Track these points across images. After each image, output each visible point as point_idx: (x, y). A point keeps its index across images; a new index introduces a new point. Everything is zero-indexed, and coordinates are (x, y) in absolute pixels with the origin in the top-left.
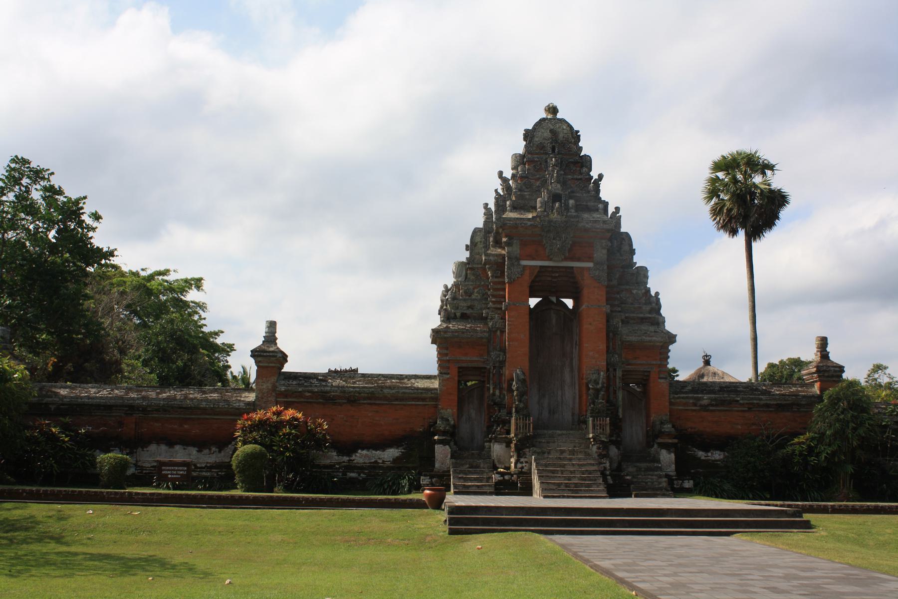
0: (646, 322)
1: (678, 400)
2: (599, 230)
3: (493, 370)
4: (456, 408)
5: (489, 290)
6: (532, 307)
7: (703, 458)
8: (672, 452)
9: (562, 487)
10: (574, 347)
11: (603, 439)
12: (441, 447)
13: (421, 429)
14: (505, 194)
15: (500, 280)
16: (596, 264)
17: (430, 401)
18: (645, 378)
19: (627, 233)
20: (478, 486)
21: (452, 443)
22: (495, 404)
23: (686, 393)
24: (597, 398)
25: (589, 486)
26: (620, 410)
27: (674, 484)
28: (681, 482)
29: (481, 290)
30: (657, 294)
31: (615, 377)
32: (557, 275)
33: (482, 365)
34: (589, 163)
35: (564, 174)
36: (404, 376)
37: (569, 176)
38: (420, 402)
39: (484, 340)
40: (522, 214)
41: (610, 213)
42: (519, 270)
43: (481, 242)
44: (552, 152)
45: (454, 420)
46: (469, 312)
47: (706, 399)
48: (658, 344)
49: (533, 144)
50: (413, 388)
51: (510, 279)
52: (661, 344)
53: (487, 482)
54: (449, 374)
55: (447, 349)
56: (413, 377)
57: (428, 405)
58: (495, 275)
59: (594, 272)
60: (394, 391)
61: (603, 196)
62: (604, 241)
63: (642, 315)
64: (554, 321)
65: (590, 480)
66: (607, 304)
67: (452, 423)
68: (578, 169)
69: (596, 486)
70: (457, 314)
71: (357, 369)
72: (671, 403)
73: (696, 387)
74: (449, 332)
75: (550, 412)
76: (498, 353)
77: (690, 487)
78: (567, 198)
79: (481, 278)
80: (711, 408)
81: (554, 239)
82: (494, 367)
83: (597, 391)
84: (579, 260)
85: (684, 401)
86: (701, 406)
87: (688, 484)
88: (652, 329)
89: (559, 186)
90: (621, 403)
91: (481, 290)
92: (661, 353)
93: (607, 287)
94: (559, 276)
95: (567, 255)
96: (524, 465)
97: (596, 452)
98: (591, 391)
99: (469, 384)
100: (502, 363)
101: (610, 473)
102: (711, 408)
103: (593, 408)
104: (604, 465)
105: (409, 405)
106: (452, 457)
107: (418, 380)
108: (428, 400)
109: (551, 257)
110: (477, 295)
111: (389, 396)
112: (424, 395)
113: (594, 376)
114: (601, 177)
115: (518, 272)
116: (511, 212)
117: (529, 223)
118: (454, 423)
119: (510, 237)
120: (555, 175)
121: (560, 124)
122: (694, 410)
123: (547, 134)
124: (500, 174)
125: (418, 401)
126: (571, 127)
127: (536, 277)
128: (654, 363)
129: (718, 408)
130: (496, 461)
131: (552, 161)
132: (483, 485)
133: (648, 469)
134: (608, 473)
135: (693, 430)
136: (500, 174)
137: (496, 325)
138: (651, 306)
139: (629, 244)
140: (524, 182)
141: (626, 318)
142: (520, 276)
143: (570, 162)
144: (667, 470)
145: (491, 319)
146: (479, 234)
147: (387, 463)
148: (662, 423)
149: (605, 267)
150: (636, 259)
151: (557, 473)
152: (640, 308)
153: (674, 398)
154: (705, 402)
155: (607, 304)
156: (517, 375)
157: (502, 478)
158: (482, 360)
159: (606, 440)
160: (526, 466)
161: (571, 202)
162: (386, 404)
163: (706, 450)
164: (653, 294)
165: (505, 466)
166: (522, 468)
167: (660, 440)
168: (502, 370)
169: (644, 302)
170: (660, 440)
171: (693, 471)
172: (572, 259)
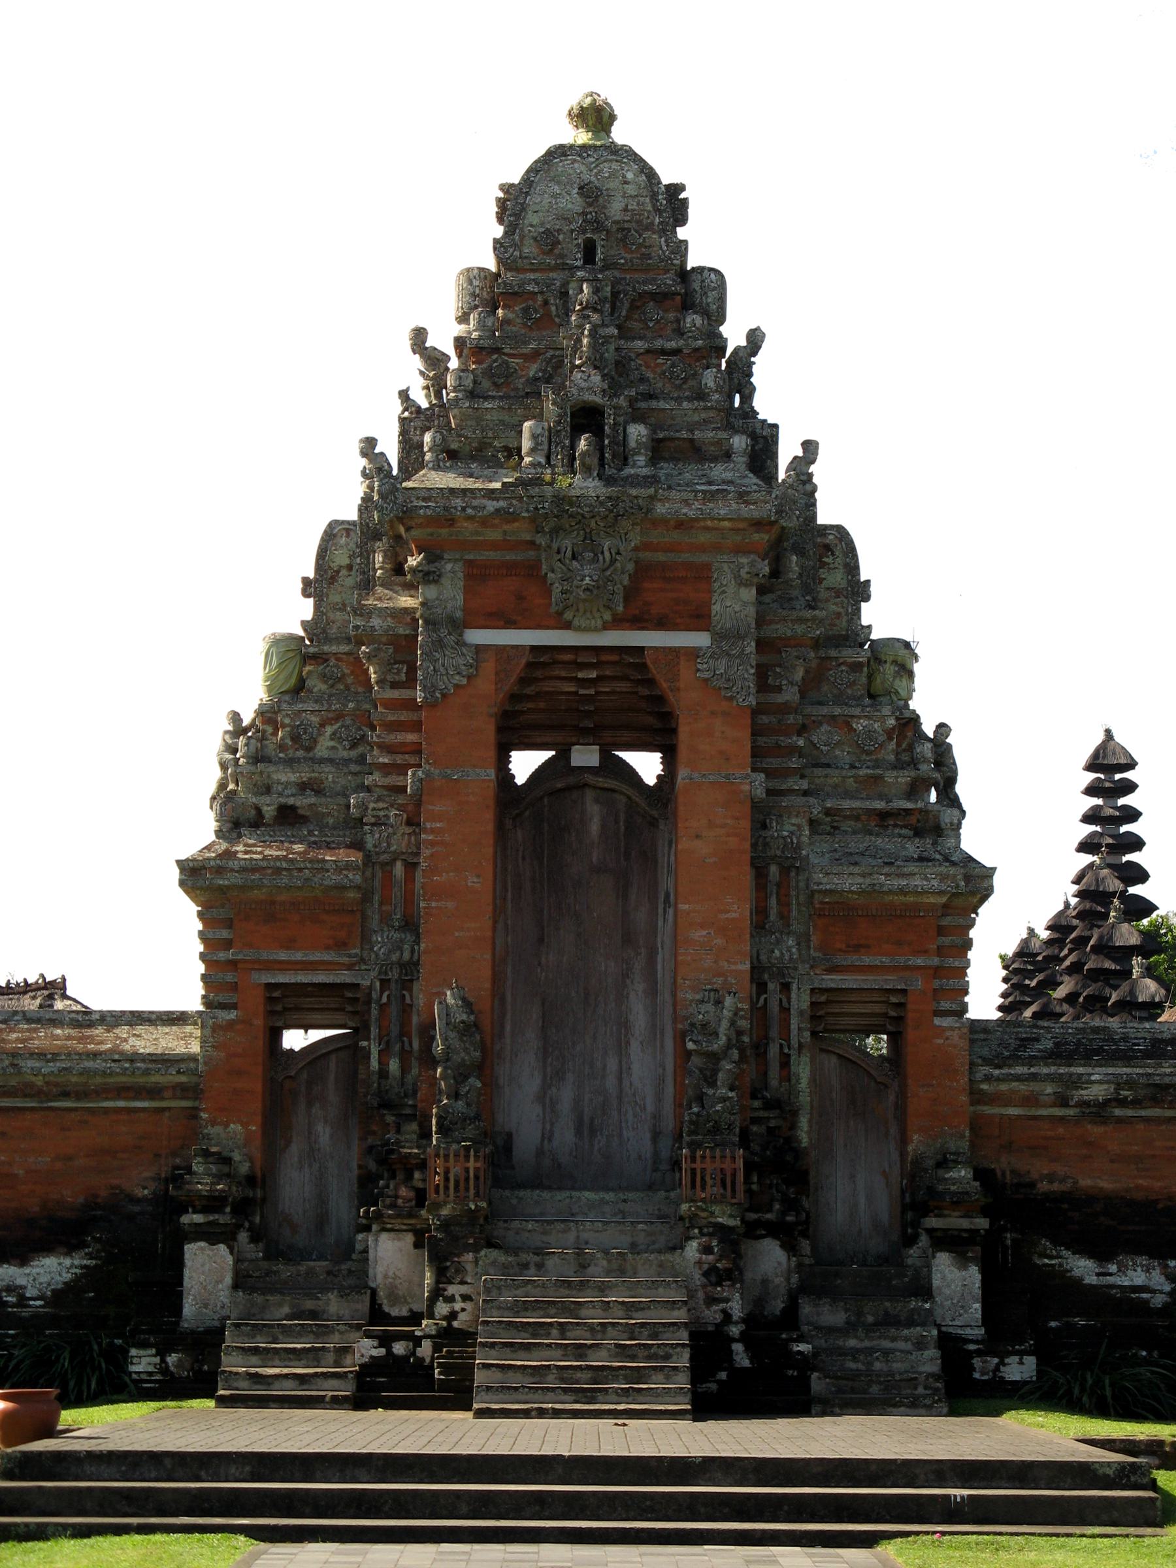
0: (895, 826)
1: (1004, 1087)
2: (726, 524)
3: (382, 992)
4: (259, 1119)
5: (373, 728)
6: (520, 780)
7: (1092, 1280)
8: (972, 1260)
9: (551, 1382)
10: (661, 911)
11: (720, 1220)
12: (202, 1249)
13: (146, 1192)
14: (432, 406)
15: (403, 694)
16: (719, 637)
17: (174, 1097)
18: (893, 1013)
19: (841, 533)
20: (302, 1379)
21: (243, 1236)
22: (386, 1105)
23: (1031, 1061)
24: (713, 1084)
25: (639, 1375)
26: (804, 1122)
27: (974, 1369)
28: (996, 1360)
29: (347, 727)
30: (943, 729)
31: (785, 1010)
32: (593, 675)
33: (345, 977)
34: (713, 295)
35: (620, 337)
36: (95, 1017)
37: (639, 343)
38: (143, 1099)
39: (352, 895)
40: (471, 476)
41: (784, 461)
42: (461, 661)
43: (350, 567)
44: (585, 262)
45: (251, 1160)
46: (302, 802)
47: (1100, 1082)
48: (932, 900)
49: (522, 238)
50: (116, 1057)
51: (432, 693)
52: (944, 899)
53: (337, 1364)
54: (234, 1006)
55: (229, 924)
56: (128, 1017)
57: (169, 1109)
58: (389, 678)
59: (711, 662)
60: (52, 1067)
61: (765, 407)
62: (744, 560)
63: (879, 805)
64: (595, 827)
65: (649, 1358)
66: (754, 770)
67: (244, 1169)
68: (671, 316)
69: (660, 1377)
70: (265, 809)
71: (64, 979)
72: (977, 1097)
73: (1067, 1043)
74: (232, 870)
75: (579, 1132)
76: (397, 935)
77: (1026, 1376)
78: (621, 419)
79: (347, 688)
80: (1118, 1112)
81: (574, 557)
82: (382, 981)
83: (714, 1058)
84: (662, 624)
85: (1022, 1087)
86: (1083, 1104)
87: (1020, 1369)
88: (912, 848)
89: (596, 378)
90: (804, 1098)
91: (347, 727)
92: (941, 931)
93: (756, 712)
94: (599, 678)
95: (621, 609)
96: (458, 1306)
97: (699, 1263)
98: (696, 1060)
99: (294, 1039)
100: (409, 971)
101: (742, 1333)
102: (1118, 1112)
103: (698, 1115)
104: (722, 1306)
105: (106, 1111)
106: (236, 1286)
107: (140, 1029)
108: (166, 1094)
109: (568, 615)
110: (332, 743)
111: (39, 1081)
112: (155, 1078)
113: (704, 1008)
114: (755, 339)
115: (456, 668)
116: (437, 467)
117: (491, 505)
118: (252, 1168)
119: (433, 555)
120: (585, 341)
121: (615, 166)
122: (1062, 1119)
123: (572, 202)
124: (419, 337)
125: (134, 1099)
126: (650, 175)
127: (523, 681)
128: (920, 961)
129: (1143, 1113)
130: (381, 1293)
131: (582, 291)
132: (316, 1375)
133: (889, 1321)
134: (735, 1331)
135: (1056, 1187)
136: (419, 337)
137: (389, 845)
138: (913, 773)
139: (846, 565)
140: (484, 366)
141: (828, 812)
142: (465, 681)
143: (645, 292)
144: (957, 1323)
145: (373, 825)
146: (343, 540)
147: (32, 1303)
148: (943, 1163)
149: (751, 647)
150: (869, 614)
151: (548, 1336)
152: (877, 779)
153: (988, 1078)
154: (1097, 1092)
155: (754, 770)
156: (447, 1011)
157: (382, 1351)
158: (346, 960)
159: (731, 1222)
160: (463, 1310)
161: (637, 432)
162: (32, 1109)
163: (1102, 1253)
164: (929, 729)
165: (411, 1310)
166: (453, 1315)
167: (932, 1222)
168: (410, 990)
169: (892, 757)
170: (932, 1222)
171: (1053, 1324)
172: (638, 622)
